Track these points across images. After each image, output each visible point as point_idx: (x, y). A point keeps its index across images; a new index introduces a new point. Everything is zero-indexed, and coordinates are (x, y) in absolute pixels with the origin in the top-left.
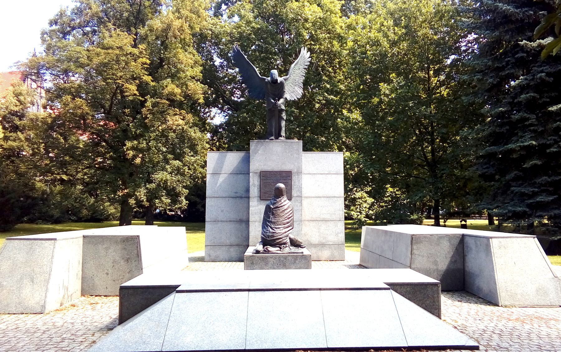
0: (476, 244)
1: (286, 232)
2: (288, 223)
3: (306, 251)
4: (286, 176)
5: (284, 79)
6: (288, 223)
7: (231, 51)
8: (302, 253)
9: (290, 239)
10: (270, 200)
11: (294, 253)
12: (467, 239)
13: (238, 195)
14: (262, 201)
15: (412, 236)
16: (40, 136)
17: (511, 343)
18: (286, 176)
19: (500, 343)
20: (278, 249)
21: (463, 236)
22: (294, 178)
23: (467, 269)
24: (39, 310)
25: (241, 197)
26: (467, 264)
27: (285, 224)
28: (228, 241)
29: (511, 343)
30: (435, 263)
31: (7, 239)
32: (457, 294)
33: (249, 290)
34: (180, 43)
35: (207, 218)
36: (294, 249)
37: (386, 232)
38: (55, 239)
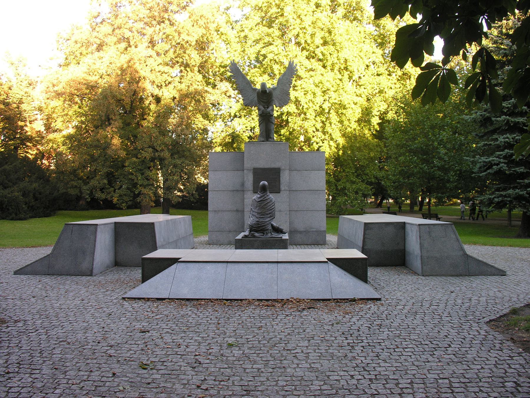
2: (270, 213)
6: (270, 213)
7: (515, 52)
8: (281, 237)
15: (366, 224)
16: (383, 154)
20: (262, 234)
22: (281, 172)
23: (406, 249)
25: (237, 191)
26: (407, 246)
27: (267, 215)
28: (227, 228)
31: (417, 231)
33: (227, 262)
35: (209, 209)
36: (275, 235)
37: (350, 220)
38: (97, 225)
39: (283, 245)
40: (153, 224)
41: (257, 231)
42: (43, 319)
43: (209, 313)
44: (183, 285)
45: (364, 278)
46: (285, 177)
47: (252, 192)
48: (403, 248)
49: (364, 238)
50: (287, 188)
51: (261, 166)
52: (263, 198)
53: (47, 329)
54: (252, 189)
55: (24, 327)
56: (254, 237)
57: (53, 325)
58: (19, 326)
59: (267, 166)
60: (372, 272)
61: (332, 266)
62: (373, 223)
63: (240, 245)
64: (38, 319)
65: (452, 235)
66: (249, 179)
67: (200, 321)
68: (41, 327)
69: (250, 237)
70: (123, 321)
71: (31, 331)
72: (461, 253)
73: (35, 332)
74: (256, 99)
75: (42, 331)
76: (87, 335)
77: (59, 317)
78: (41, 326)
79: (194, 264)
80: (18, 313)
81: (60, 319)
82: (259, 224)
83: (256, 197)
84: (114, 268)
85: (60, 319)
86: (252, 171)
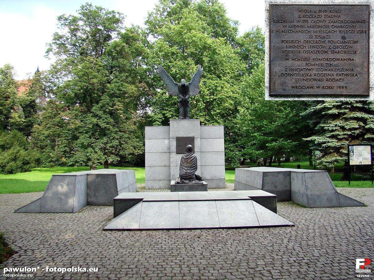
0: (297, 176)
1: (193, 172)
3: (204, 183)
4: (191, 140)
5: (188, 84)
9: (195, 175)
10: (184, 154)
11: (198, 183)
12: (292, 174)
13: (163, 151)
14: (178, 155)
17: (310, 223)
18: (191, 140)
19: (305, 223)
20: (189, 181)
21: (290, 172)
23: (292, 189)
24: (71, 211)
26: (292, 187)
27: (192, 168)
29: (310, 223)
30: (276, 187)
32: (286, 203)
34: (141, 81)
35: (146, 165)
36: (197, 181)
38: (76, 176)
39: (204, 188)
40: (115, 175)
41: (185, 179)
42: (48, 249)
43: (175, 240)
44: (148, 218)
45: (275, 211)
46: (197, 143)
47: (175, 153)
48: (289, 189)
49: (263, 183)
50: (199, 151)
51: (182, 136)
52: (189, 156)
53: (52, 257)
54: (176, 151)
55: (34, 256)
56: (184, 183)
57: (57, 254)
58: (29, 254)
59: (185, 136)
60: (280, 206)
61: (250, 202)
62: (269, 172)
63: (174, 188)
64: (43, 248)
65: (327, 179)
66: (174, 143)
67: (171, 247)
68: (47, 255)
69: (181, 184)
70: (111, 249)
71: (40, 259)
72: (334, 191)
73: (43, 260)
74: (177, 90)
75: (49, 259)
76: (87, 261)
77: (60, 246)
78: (47, 254)
79: (155, 203)
80: (26, 244)
81: (61, 248)
82: (187, 174)
83: (180, 157)
84: (87, 207)
85: (61, 248)
86: (175, 139)
